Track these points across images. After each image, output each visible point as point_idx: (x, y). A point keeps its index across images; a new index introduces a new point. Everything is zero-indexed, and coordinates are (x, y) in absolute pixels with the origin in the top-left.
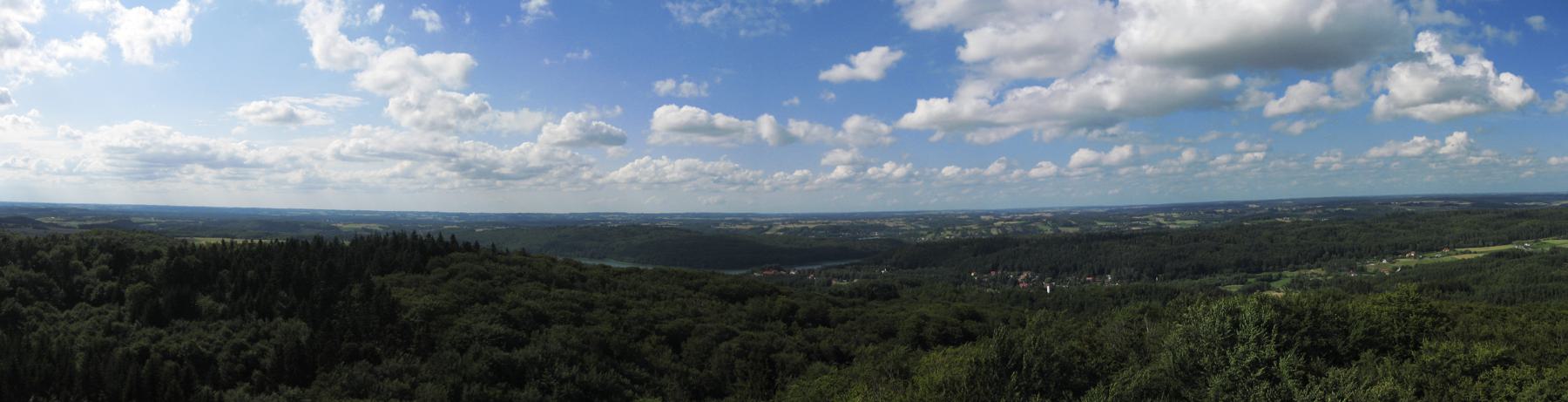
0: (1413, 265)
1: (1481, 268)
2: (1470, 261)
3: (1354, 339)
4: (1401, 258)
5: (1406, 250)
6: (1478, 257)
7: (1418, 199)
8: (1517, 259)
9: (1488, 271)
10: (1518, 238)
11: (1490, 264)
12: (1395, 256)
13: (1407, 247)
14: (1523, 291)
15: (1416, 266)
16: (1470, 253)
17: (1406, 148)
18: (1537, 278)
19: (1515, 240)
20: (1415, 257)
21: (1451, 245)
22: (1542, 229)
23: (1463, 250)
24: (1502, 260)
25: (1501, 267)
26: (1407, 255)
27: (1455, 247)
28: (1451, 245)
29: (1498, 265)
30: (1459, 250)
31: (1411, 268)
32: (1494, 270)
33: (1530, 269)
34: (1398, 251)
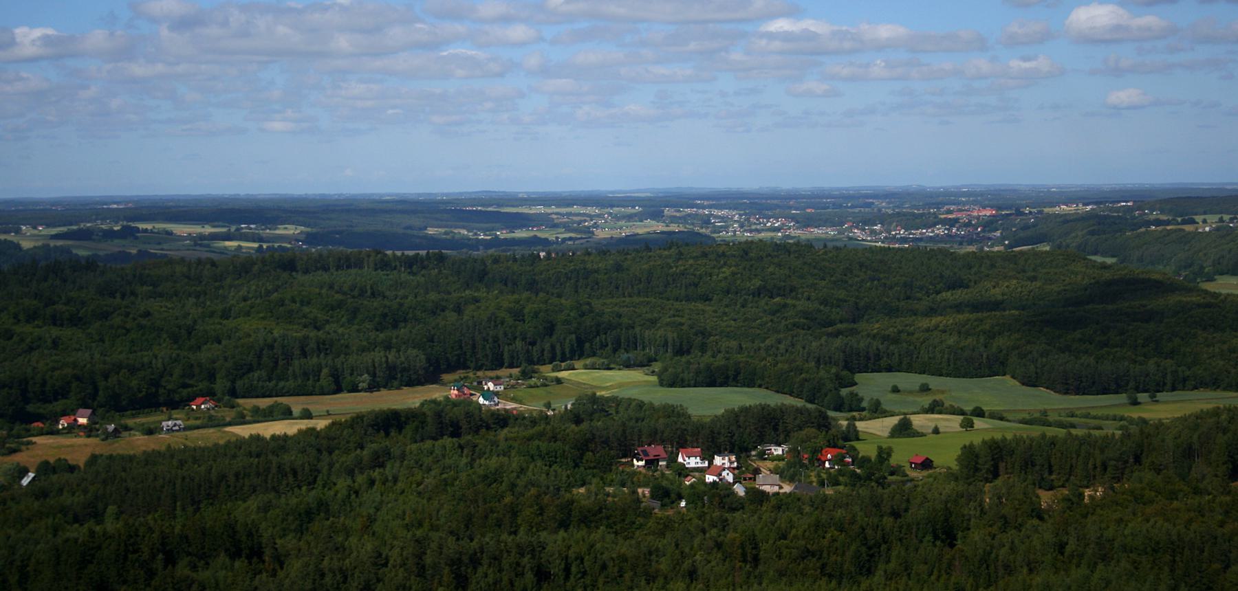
0: (80, 459)
1: (315, 471)
2: (281, 442)
3: (300, 369)
4: (41, 433)
5: (58, 406)
6: (311, 431)
7: (115, 215)
8: (447, 441)
9: (342, 484)
10: (459, 364)
11: (349, 459)
12: (18, 428)
13: (61, 393)
14: (455, 563)
15: (94, 459)
16: (287, 414)
17: (636, 385)
18: (514, 512)
19: (451, 369)
20: (89, 431)
21: (220, 385)
22: (550, 329)
23: (264, 403)
24: (398, 442)
25: (389, 470)
26: (63, 423)
27: (234, 393)
28: (220, 385)
29: (378, 461)
30: (247, 403)
31: (72, 469)
32: (361, 479)
33: (492, 478)
34: (30, 408)
